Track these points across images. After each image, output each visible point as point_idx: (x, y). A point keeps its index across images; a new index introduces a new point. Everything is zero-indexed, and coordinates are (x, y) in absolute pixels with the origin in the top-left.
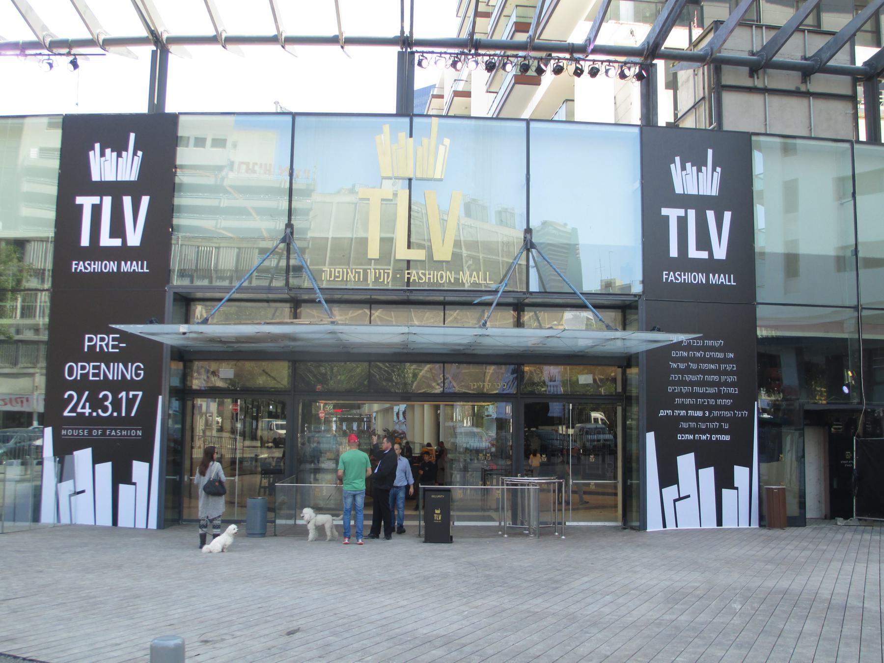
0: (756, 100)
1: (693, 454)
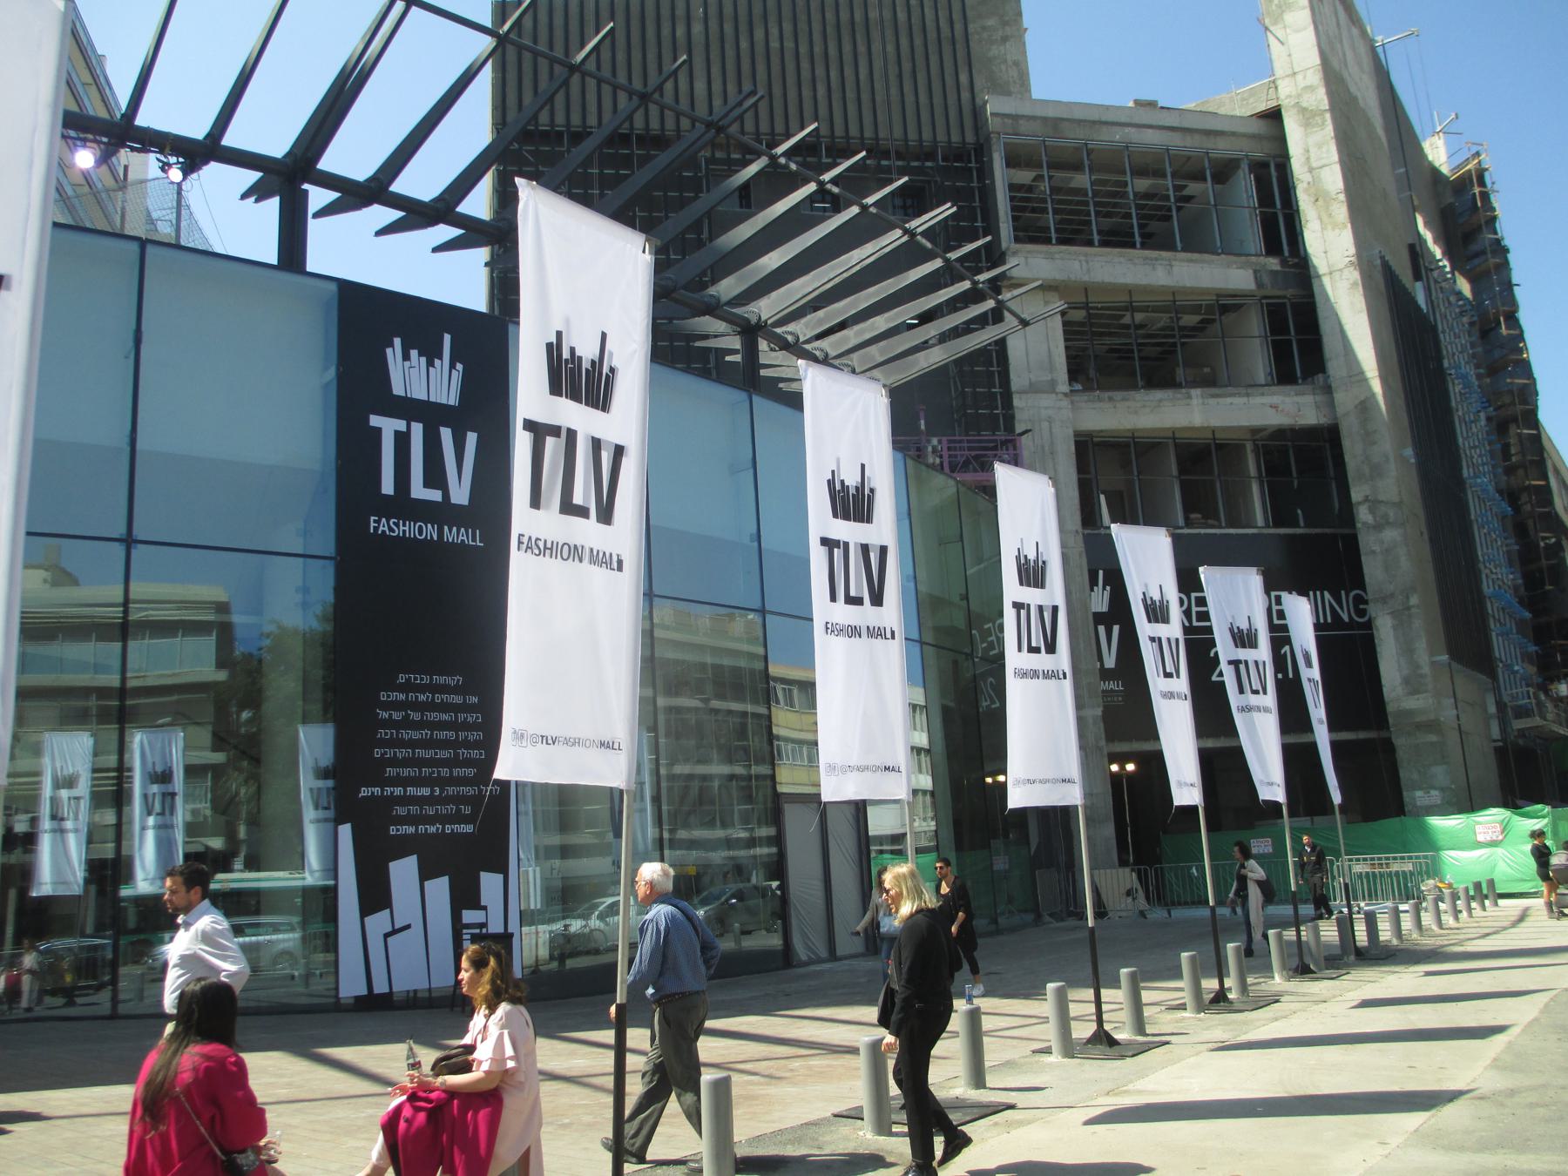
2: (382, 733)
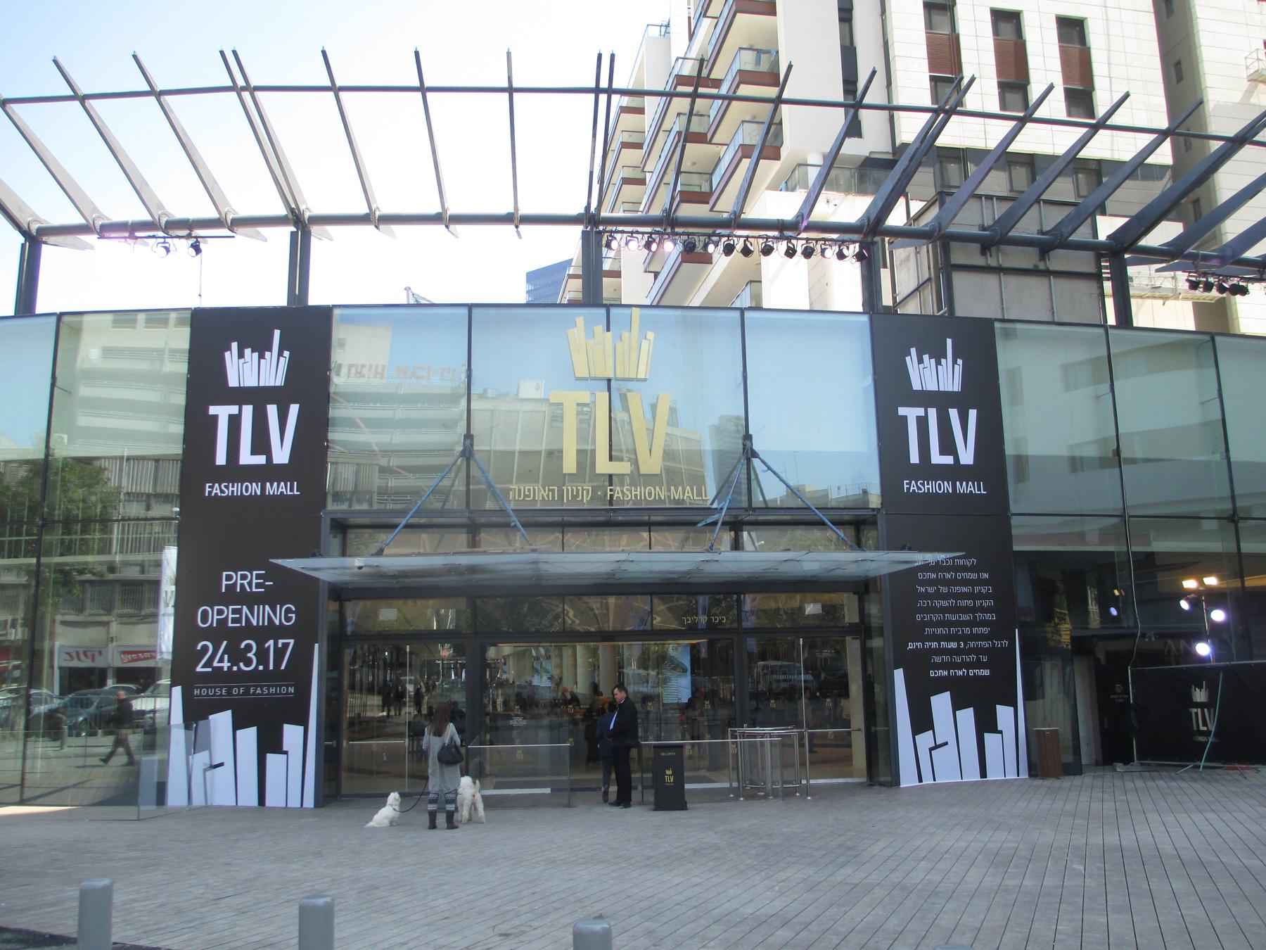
0: (991, 280)
1: (948, 694)
2: (922, 603)
